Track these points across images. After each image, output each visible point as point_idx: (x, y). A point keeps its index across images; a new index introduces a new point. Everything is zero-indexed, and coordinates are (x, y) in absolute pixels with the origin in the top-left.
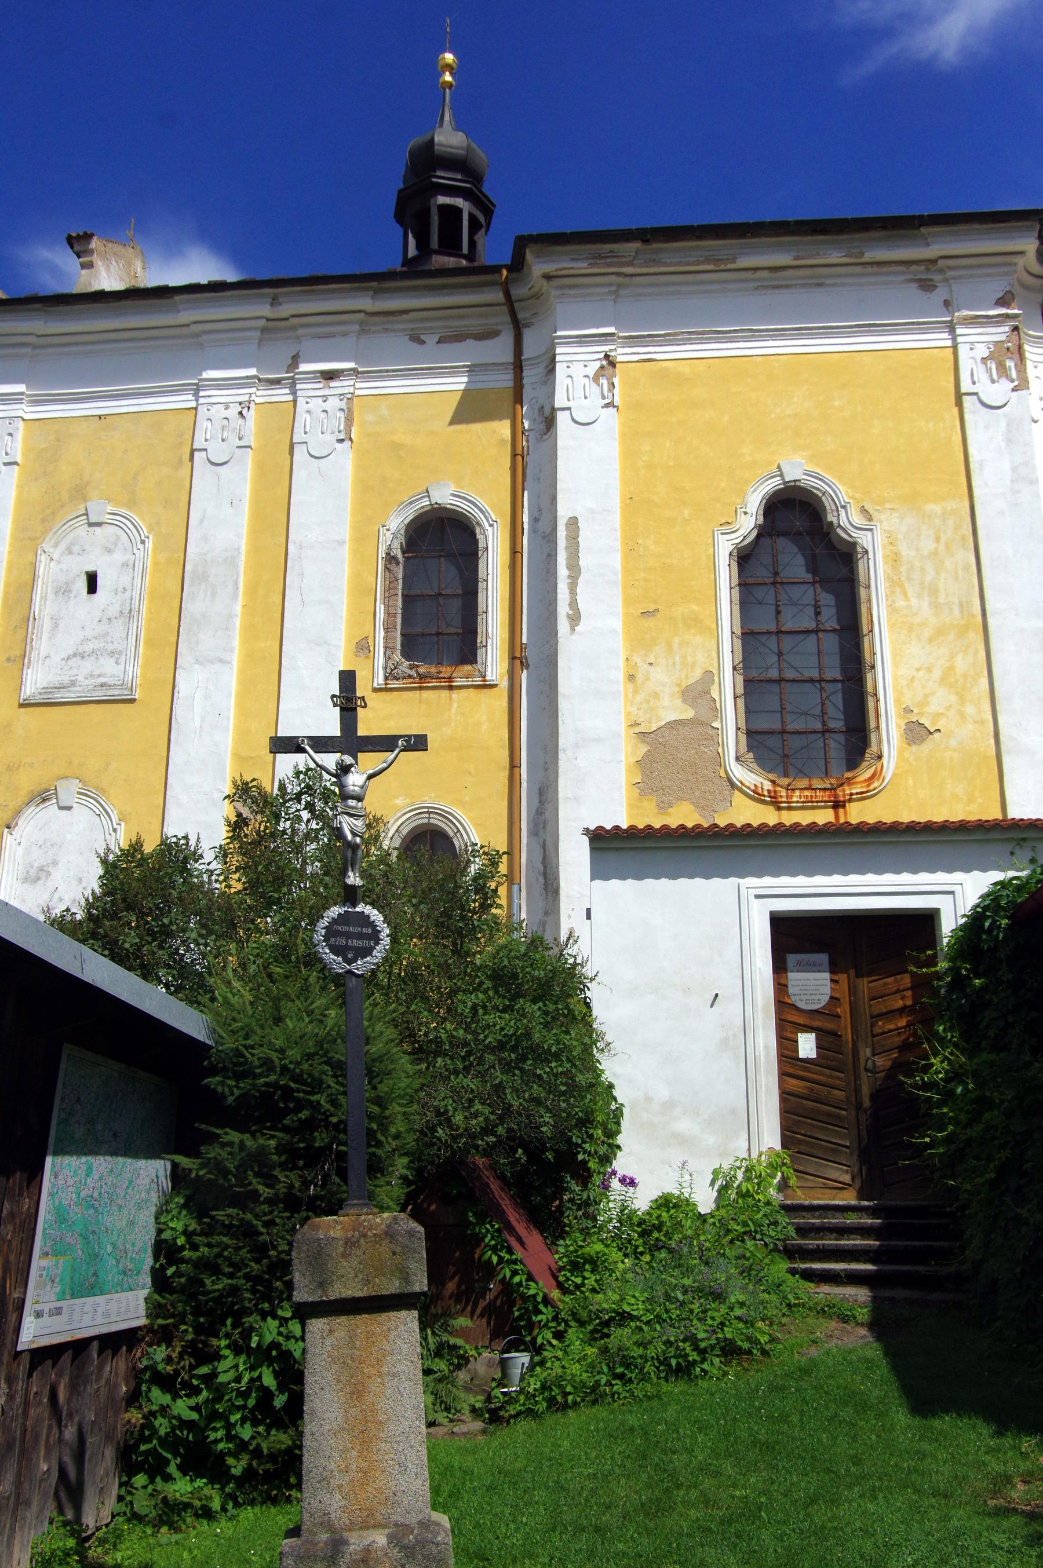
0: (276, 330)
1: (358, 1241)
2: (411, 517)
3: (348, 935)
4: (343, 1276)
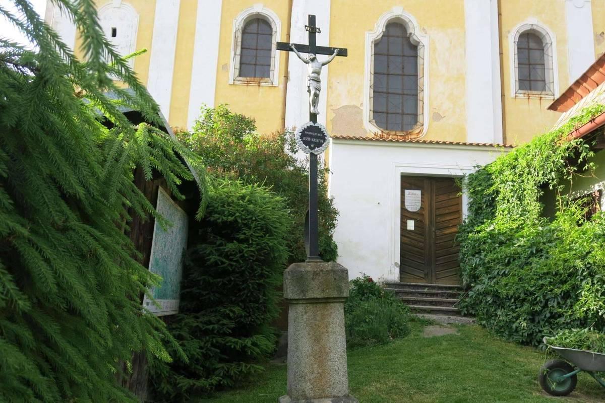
1: (319, 273)
2: (246, 17)
3: (311, 136)
4: (312, 288)
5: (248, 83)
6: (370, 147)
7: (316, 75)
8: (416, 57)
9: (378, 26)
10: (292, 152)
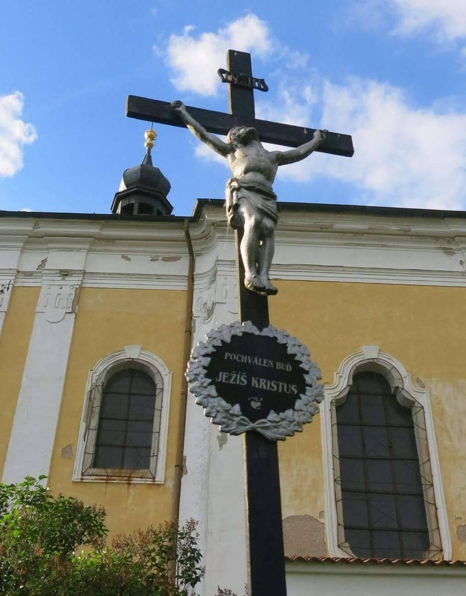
0: (33, 243)
2: (111, 366)
3: (251, 371)
5: (108, 480)
6: (358, 579)
7: (259, 177)
8: (411, 427)
9: (341, 377)
10: (186, 582)
